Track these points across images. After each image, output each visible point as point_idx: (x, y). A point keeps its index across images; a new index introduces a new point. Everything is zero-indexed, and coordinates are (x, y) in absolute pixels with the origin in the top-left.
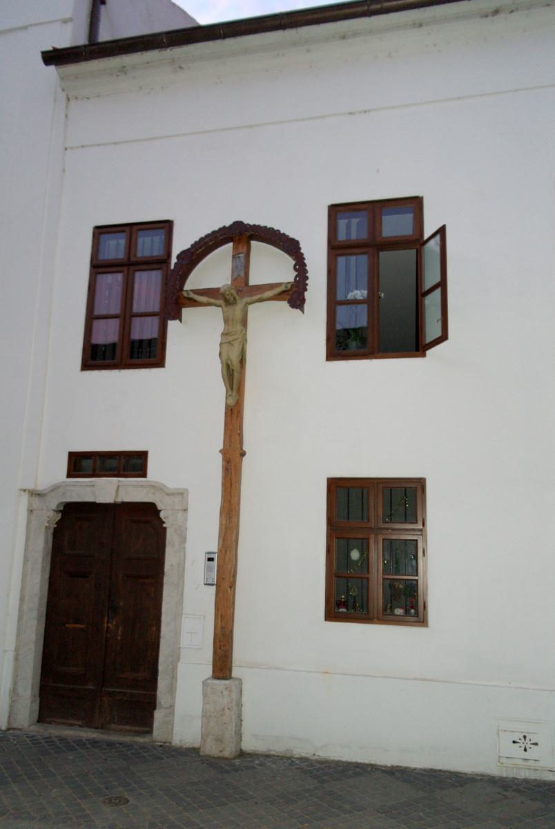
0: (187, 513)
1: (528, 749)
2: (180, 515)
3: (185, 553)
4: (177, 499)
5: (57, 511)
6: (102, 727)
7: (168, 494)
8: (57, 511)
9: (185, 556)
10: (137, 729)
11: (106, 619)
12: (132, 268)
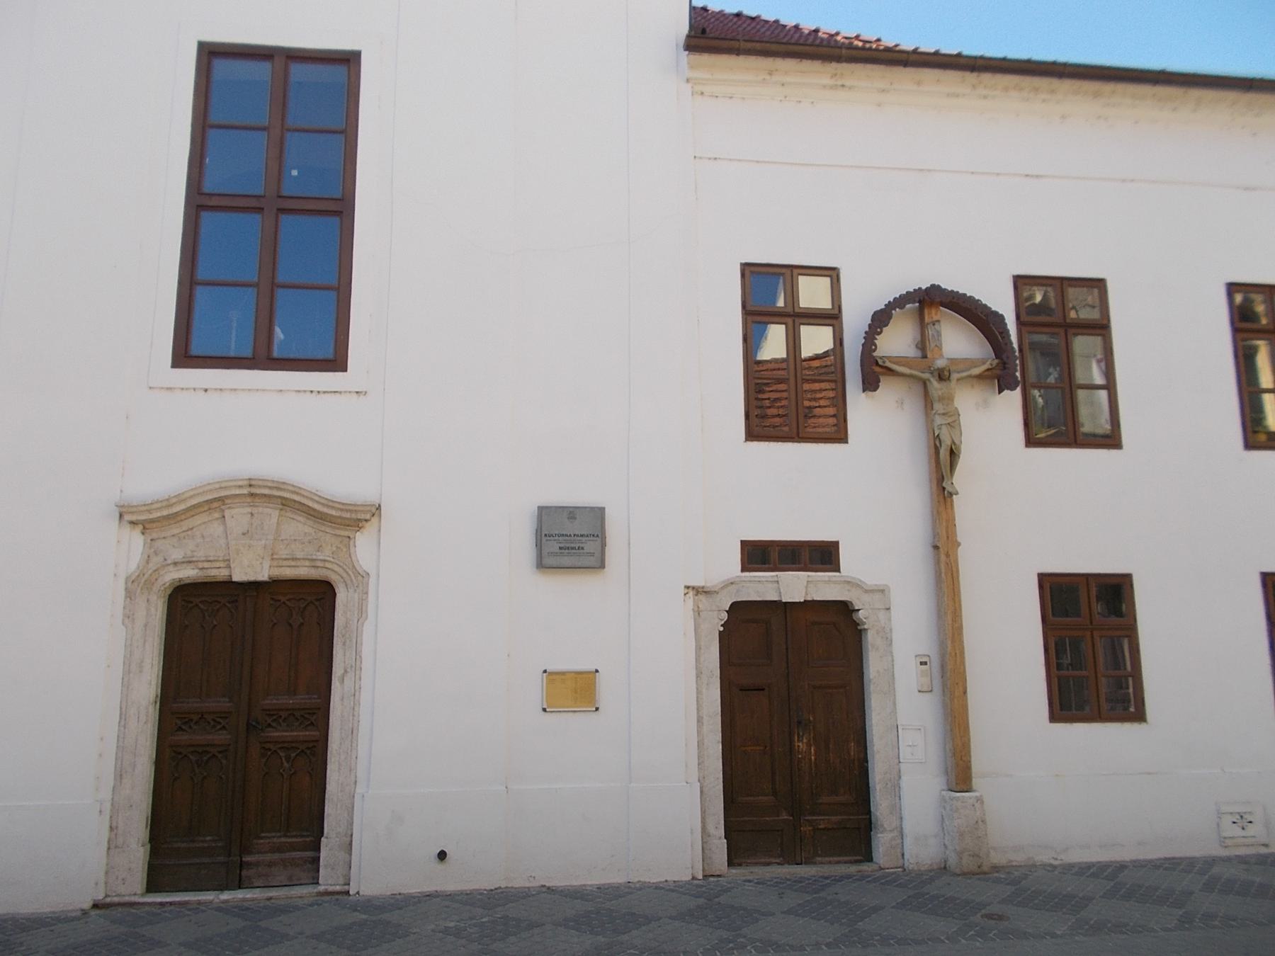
0: (890, 612)
1: (1245, 827)
2: (882, 615)
3: (892, 656)
4: (877, 596)
5: (866, 630)
6: (808, 861)
7: (866, 591)
8: (866, 630)
9: (893, 661)
10: (831, 859)
11: (796, 737)
12: (798, 320)
